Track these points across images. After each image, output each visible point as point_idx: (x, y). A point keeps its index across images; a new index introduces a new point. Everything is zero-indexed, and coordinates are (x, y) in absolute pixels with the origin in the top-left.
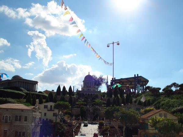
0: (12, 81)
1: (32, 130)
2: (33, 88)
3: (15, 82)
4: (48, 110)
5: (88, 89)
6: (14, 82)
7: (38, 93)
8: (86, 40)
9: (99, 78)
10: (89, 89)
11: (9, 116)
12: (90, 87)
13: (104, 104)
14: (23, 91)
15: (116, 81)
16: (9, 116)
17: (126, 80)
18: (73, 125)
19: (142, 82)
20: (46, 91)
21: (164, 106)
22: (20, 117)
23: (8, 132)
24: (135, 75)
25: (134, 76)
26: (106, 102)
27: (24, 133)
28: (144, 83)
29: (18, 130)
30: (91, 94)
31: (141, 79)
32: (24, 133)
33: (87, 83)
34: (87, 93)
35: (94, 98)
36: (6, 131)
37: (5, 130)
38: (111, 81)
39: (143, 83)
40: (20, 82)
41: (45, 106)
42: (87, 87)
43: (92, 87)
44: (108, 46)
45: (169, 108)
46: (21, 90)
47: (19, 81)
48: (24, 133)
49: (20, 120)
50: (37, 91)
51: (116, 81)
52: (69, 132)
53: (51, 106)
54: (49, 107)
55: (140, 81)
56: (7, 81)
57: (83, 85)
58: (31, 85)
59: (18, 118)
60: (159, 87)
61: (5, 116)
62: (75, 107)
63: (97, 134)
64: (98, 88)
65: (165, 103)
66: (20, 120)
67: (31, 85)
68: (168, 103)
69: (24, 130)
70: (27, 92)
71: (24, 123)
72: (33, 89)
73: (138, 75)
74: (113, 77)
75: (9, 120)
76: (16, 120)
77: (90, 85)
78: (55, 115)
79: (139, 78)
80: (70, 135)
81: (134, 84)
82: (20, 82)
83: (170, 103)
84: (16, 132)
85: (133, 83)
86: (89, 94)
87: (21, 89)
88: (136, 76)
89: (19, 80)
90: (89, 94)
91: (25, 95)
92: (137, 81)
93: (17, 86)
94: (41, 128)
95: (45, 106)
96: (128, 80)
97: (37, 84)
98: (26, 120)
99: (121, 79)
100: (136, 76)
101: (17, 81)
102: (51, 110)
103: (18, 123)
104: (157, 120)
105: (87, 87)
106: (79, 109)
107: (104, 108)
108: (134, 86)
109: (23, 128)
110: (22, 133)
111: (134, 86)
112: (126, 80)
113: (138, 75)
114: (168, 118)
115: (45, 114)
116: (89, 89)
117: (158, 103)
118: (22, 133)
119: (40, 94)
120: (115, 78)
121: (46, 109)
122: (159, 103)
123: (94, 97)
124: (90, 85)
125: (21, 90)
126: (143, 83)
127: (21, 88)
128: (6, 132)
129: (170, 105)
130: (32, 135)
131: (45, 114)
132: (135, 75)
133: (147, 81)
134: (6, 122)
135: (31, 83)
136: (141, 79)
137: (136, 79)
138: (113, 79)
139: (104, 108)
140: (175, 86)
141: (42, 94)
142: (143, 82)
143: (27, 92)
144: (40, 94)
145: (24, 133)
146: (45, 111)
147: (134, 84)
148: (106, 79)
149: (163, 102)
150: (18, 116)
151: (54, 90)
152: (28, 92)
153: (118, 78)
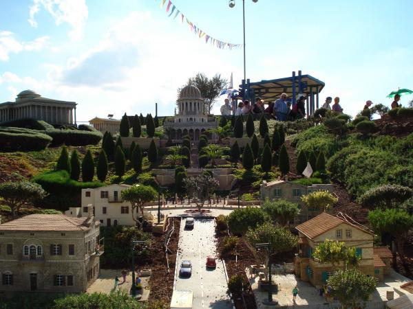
0: (17, 106)
1: (86, 268)
2: (68, 116)
3: (26, 107)
4: (110, 202)
5: (189, 118)
6: (23, 107)
7: (79, 132)
8: (174, 8)
9: (212, 79)
10: (191, 119)
11: (36, 247)
12: (195, 113)
13: (226, 153)
14: (45, 129)
15: (251, 87)
16: (36, 247)
17: (274, 85)
18: (166, 232)
19: (309, 88)
20: (96, 122)
21: (353, 166)
22: (60, 246)
23: (38, 277)
24: (294, 73)
25: (291, 75)
26: (230, 149)
28: (314, 89)
29: (58, 272)
30: (197, 130)
31: (306, 82)
32: (70, 278)
33: (187, 103)
34: (188, 129)
35: (203, 144)
36: (36, 274)
37: (32, 274)
38: (240, 86)
39: (311, 90)
40: (36, 108)
41: (102, 192)
42: (188, 113)
43: (198, 112)
44: (232, 6)
45: (363, 173)
46: (41, 128)
47: (33, 106)
49: (60, 253)
50: (76, 124)
51: (251, 87)
52: (156, 252)
53: (116, 193)
54: (111, 195)
55: (306, 85)
56: (6, 107)
58: (61, 111)
59: (56, 250)
60: (348, 114)
61: (29, 247)
62: (164, 168)
63: (215, 260)
64: (210, 103)
65: (354, 158)
66: (60, 253)
67: (61, 111)
68: (362, 160)
69: (71, 272)
70: (53, 130)
71: (70, 259)
72: (68, 120)
73: (300, 72)
75: (38, 254)
76: (53, 253)
77: (193, 110)
78: (124, 210)
79: (303, 80)
80: (159, 261)
81: (291, 91)
82: (36, 108)
83: (367, 162)
84: (56, 277)
85: (289, 90)
86: (191, 130)
87: (40, 124)
88: (297, 75)
89: (34, 103)
90: (191, 130)
91: (51, 138)
92: (297, 84)
93: (31, 116)
94: (100, 260)
95: (102, 192)
97: (75, 109)
98: (72, 252)
99: (263, 82)
100: (297, 75)
101: (29, 106)
102: (116, 201)
103: (56, 259)
104: (331, 251)
105: (188, 113)
106: (173, 172)
107: (225, 167)
108: (292, 94)
109: (69, 267)
110: (66, 278)
111: (292, 94)
112: (274, 85)
113: (300, 72)
114: (354, 238)
115: (105, 210)
116: (191, 119)
117: (341, 158)
118: (66, 278)
119: (84, 132)
120: (248, 80)
121: (106, 200)
122: (344, 156)
123: (203, 139)
124: (193, 110)
125: (41, 128)
126: (311, 90)
127: (40, 122)
129: (367, 165)
130: (86, 279)
131: (105, 210)
132: (294, 73)
133: (319, 86)
134: (33, 257)
135: (62, 106)
136: (306, 82)
137: (297, 81)
138: (244, 81)
139: (225, 167)
140: (380, 111)
141: (89, 132)
142: (312, 86)
143: (53, 130)
144: (84, 132)
145: (70, 278)
146: (104, 202)
147: (291, 91)
148: (229, 81)
149: (351, 157)
151: (112, 116)
152: (58, 130)
153: (255, 78)
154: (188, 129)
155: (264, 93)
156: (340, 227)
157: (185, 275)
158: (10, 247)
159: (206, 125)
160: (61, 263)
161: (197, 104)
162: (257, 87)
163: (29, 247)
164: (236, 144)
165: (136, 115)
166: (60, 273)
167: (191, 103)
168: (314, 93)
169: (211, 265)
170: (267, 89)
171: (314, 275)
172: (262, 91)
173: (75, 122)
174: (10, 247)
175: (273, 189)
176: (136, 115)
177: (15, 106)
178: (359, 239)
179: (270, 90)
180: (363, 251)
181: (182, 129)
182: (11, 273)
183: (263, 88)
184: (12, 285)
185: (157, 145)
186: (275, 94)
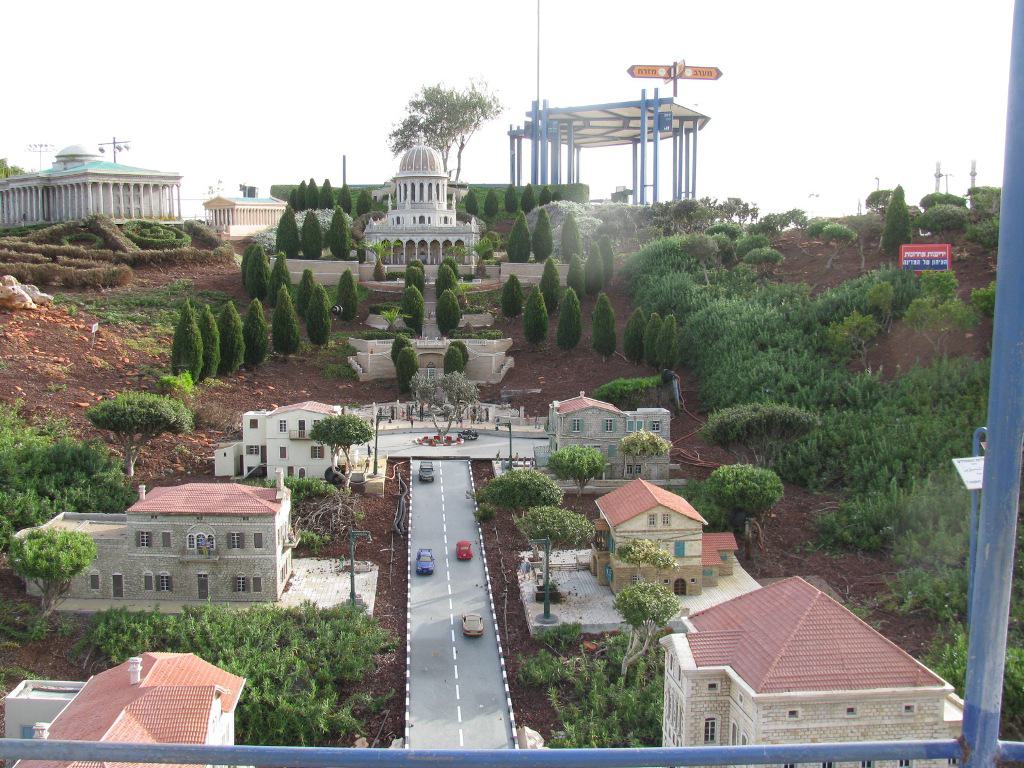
10: (422, 219)
25: (638, 98)
27: (259, 579)
28: (688, 124)
32: (257, 580)
33: (413, 186)
34: (417, 240)
36: (205, 576)
48: (259, 579)
49: (241, 545)
53: (302, 424)
54: (293, 426)
57: (444, 721)
61: (195, 536)
66: (241, 545)
69: (258, 573)
74: (536, 99)
85: (632, 124)
90: (423, 243)
96: (611, 113)
103: (236, 554)
116: (422, 219)
118: (252, 581)
121: (285, 435)
126: (681, 124)
128: (206, 581)
138: (536, 104)
142: (682, 119)
145: (257, 580)
150: (233, 535)
154: (417, 240)
155: (580, 128)
156: (654, 511)
157: (425, 573)
158: (166, 537)
159: (454, 232)
160: (243, 560)
161: (434, 188)
162: (566, 117)
163: (195, 536)
164: (513, 279)
165: (303, 183)
166: (242, 574)
167: (422, 186)
168: (688, 131)
169: (463, 555)
170: (587, 122)
171: (615, 578)
172: (575, 123)
173: (179, 213)
174: (166, 537)
175: (569, 419)
176: (303, 183)
177: (53, 183)
178: (682, 528)
179: (592, 123)
180: (687, 545)
181: (405, 239)
182: (169, 574)
183: (579, 118)
184: (171, 590)
185: (355, 275)
186: (605, 131)
